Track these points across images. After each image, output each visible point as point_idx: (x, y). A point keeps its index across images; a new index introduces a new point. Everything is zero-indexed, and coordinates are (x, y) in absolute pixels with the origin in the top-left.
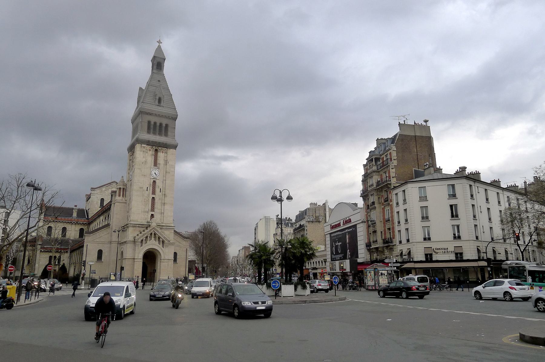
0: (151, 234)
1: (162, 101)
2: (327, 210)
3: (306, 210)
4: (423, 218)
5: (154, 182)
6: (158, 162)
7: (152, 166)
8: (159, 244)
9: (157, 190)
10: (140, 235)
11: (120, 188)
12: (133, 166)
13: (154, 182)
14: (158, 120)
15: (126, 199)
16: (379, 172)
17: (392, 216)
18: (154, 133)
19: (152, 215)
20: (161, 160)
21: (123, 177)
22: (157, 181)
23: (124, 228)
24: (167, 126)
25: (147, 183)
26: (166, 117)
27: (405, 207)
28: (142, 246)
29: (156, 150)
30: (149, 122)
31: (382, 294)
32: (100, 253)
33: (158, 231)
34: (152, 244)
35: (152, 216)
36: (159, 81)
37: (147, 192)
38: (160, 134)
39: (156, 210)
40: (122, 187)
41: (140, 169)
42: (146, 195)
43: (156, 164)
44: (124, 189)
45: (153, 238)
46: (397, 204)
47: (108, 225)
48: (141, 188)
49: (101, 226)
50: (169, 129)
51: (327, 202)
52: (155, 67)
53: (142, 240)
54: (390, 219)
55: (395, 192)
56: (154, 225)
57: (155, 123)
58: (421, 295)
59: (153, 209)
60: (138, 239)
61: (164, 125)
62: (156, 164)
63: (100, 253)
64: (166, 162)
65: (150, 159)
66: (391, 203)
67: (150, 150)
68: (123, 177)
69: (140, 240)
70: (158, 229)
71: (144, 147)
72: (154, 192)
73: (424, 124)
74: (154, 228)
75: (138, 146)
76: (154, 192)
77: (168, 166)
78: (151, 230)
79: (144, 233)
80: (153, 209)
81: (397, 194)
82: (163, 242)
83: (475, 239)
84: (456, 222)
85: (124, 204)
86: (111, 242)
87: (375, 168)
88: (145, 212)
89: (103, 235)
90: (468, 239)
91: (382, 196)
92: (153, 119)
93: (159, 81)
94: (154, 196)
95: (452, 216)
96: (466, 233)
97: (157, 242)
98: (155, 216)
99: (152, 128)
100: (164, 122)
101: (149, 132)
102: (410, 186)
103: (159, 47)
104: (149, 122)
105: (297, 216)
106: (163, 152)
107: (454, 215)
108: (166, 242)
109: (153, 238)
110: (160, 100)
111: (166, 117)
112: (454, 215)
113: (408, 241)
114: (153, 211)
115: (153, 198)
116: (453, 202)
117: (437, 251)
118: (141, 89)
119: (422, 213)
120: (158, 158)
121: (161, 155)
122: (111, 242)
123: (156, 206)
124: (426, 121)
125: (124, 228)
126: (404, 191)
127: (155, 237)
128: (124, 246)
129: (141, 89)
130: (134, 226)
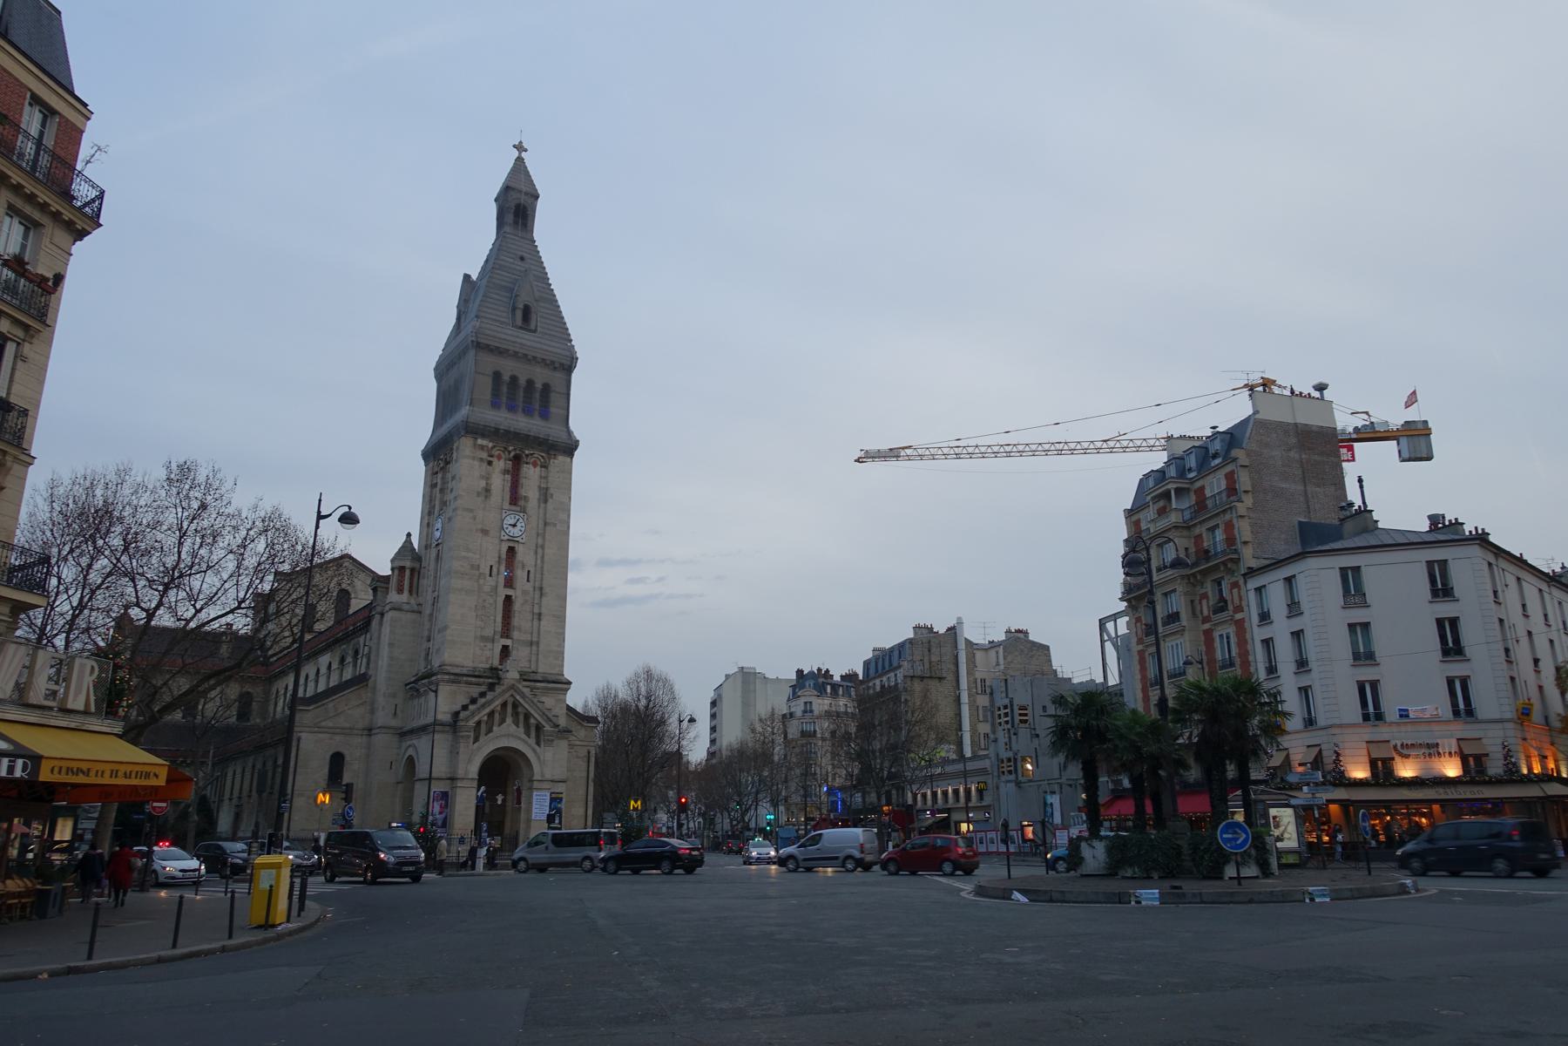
0: (504, 705)
1: (533, 317)
2: (962, 645)
3: (901, 646)
4: (1356, 656)
5: (511, 550)
6: (523, 492)
7: (506, 505)
8: (528, 734)
9: (520, 575)
10: (472, 707)
11: (402, 569)
12: (444, 504)
13: (511, 550)
14: (524, 372)
15: (420, 600)
16: (1189, 528)
17: (1244, 654)
18: (511, 408)
19: (505, 649)
20: (530, 489)
21: (409, 535)
22: (520, 549)
23: (421, 683)
24: (546, 388)
25: (491, 552)
26: (544, 363)
27: (1296, 624)
28: (476, 740)
29: (517, 461)
30: (497, 376)
31: (892, 868)
32: (337, 761)
33: (523, 695)
34: (508, 736)
35: (505, 651)
36: (522, 259)
37: (491, 582)
38: (528, 412)
39: (516, 634)
40: (408, 564)
41: (471, 511)
42: (487, 588)
43: (515, 498)
44: (412, 570)
45: (509, 720)
46: (1265, 617)
47: (361, 680)
48: (472, 567)
49: (321, 687)
50: (554, 398)
51: (960, 622)
52: (510, 218)
53: (479, 723)
54: (1238, 661)
55: (1253, 583)
56: (512, 675)
57: (530, 383)
58: (690, 865)
59: (506, 631)
60: (467, 719)
61: (539, 386)
62: (515, 498)
63: (337, 761)
64: (545, 495)
65: (499, 483)
66: (1238, 616)
67: (499, 458)
68: (409, 535)
69: (472, 723)
70: (526, 691)
71: (482, 447)
72: (509, 583)
73: (1316, 394)
74: (512, 687)
75: (465, 446)
76: (509, 583)
77: (550, 505)
78: (504, 692)
79: (483, 700)
80: (506, 631)
81: (1259, 590)
82: (539, 728)
83: (1450, 715)
84: (1457, 669)
85: (414, 616)
86: (370, 731)
87: (1174, 518)
88: (484, 639)
89: (350, 710)
90: (1497, 716)
91: (1205, 596)
92: (508, 367)
93: (522, 259)
94: (510, 592)
95: (1446, 652)
96: (1489, 699)
97: (522, 729)
98: (514, 653)
99: (507, 391)
100: (540, 376)
101: (495, 405)
102: (1312, 563)
103: (520, 160)
104: (497, 376)
105: (867, 664)
106: (535, 465)
107: (1452, 647)
108: (547, 728)
109: (509, 720)
110: (527, 312)
111: (544, 363)
112: (1452, 647)
113: (1310, 722)
114: (508, 637)
115: (508, 599)
116: (1446, 609)
117: (1405, 752)
118: (467, 277)
119: (1354, 644)
120: (523, 481)
121: (531, 474)
122: (370, 731)
123: (516, 621)
124: (1321, 388)
125: (421, 683)
126: (1289, 580)
127: (516, 714)
128: (422, 743)
129: (467, 277)
130: (457, 678)
